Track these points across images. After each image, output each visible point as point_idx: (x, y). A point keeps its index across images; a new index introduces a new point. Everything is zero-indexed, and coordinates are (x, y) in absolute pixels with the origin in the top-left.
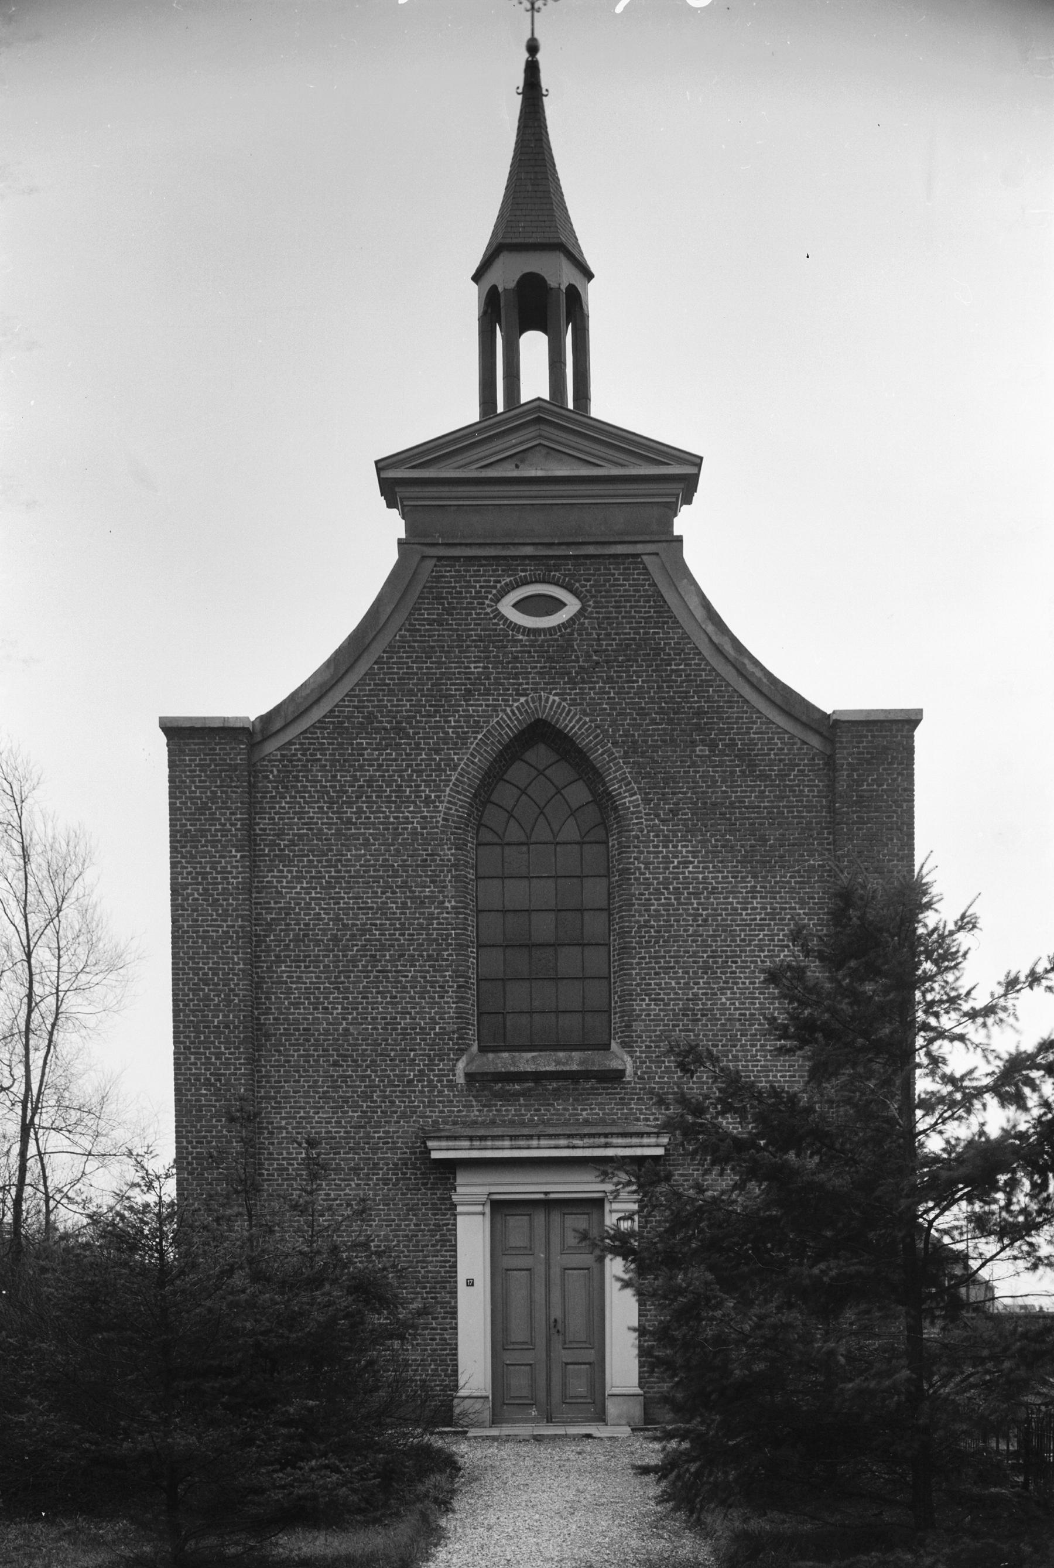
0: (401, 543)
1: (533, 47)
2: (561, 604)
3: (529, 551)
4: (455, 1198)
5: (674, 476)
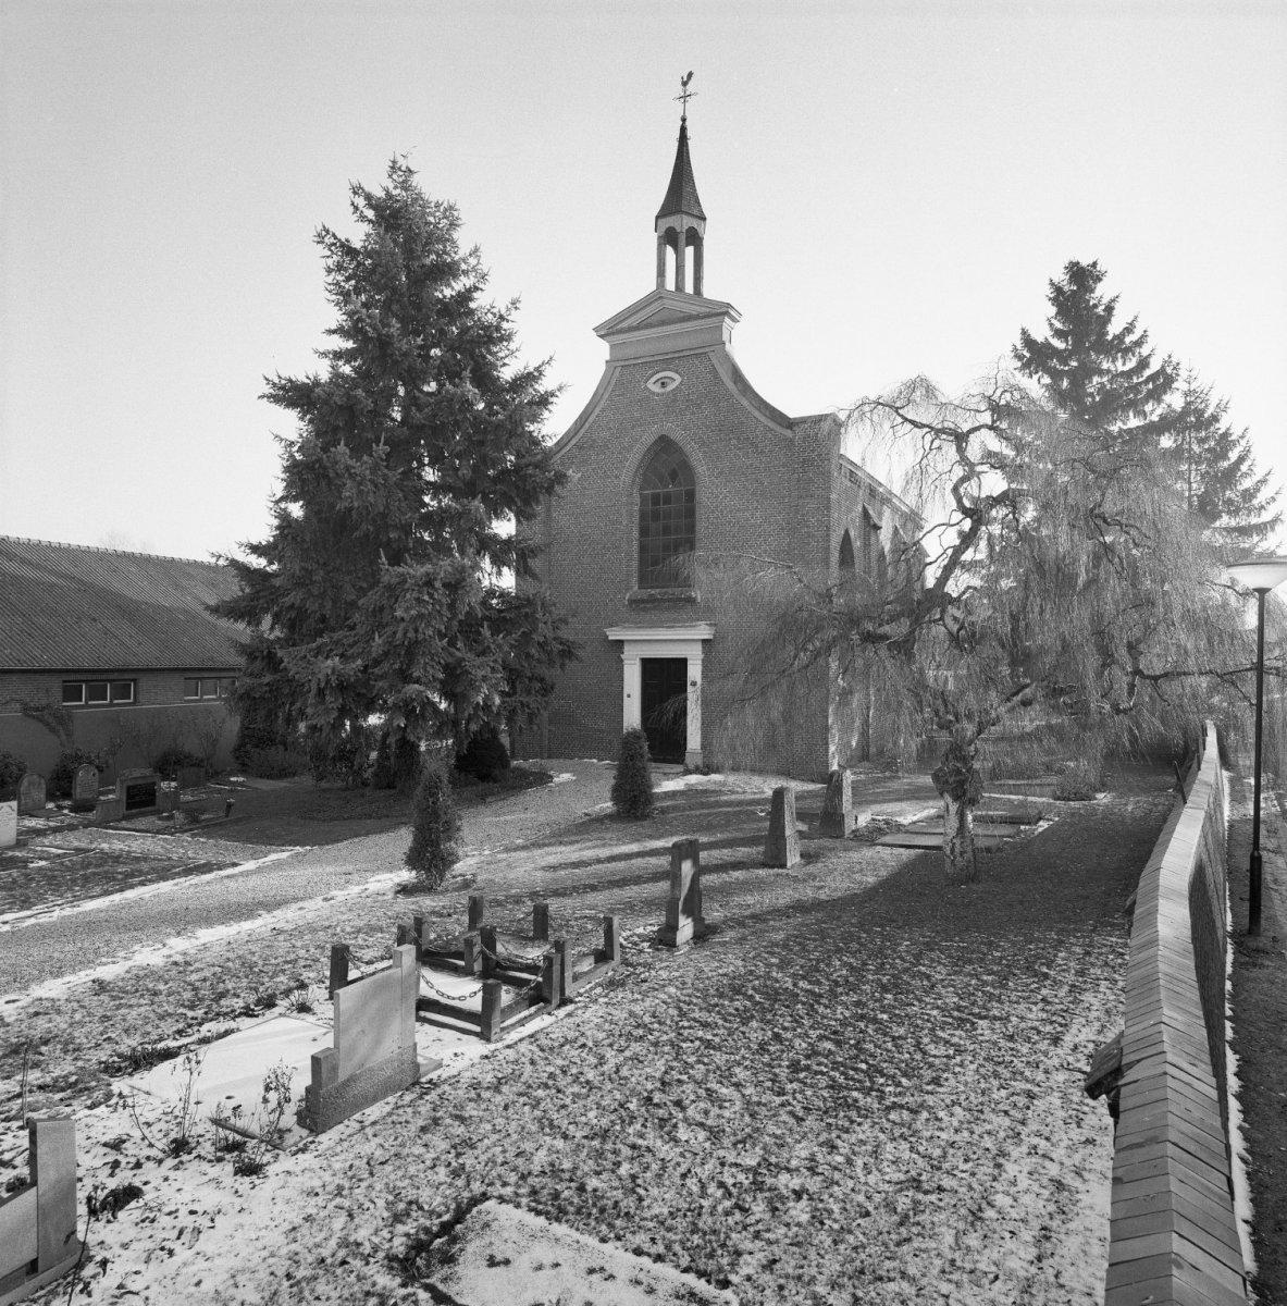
1: (684, 120)
5: (723, 311)
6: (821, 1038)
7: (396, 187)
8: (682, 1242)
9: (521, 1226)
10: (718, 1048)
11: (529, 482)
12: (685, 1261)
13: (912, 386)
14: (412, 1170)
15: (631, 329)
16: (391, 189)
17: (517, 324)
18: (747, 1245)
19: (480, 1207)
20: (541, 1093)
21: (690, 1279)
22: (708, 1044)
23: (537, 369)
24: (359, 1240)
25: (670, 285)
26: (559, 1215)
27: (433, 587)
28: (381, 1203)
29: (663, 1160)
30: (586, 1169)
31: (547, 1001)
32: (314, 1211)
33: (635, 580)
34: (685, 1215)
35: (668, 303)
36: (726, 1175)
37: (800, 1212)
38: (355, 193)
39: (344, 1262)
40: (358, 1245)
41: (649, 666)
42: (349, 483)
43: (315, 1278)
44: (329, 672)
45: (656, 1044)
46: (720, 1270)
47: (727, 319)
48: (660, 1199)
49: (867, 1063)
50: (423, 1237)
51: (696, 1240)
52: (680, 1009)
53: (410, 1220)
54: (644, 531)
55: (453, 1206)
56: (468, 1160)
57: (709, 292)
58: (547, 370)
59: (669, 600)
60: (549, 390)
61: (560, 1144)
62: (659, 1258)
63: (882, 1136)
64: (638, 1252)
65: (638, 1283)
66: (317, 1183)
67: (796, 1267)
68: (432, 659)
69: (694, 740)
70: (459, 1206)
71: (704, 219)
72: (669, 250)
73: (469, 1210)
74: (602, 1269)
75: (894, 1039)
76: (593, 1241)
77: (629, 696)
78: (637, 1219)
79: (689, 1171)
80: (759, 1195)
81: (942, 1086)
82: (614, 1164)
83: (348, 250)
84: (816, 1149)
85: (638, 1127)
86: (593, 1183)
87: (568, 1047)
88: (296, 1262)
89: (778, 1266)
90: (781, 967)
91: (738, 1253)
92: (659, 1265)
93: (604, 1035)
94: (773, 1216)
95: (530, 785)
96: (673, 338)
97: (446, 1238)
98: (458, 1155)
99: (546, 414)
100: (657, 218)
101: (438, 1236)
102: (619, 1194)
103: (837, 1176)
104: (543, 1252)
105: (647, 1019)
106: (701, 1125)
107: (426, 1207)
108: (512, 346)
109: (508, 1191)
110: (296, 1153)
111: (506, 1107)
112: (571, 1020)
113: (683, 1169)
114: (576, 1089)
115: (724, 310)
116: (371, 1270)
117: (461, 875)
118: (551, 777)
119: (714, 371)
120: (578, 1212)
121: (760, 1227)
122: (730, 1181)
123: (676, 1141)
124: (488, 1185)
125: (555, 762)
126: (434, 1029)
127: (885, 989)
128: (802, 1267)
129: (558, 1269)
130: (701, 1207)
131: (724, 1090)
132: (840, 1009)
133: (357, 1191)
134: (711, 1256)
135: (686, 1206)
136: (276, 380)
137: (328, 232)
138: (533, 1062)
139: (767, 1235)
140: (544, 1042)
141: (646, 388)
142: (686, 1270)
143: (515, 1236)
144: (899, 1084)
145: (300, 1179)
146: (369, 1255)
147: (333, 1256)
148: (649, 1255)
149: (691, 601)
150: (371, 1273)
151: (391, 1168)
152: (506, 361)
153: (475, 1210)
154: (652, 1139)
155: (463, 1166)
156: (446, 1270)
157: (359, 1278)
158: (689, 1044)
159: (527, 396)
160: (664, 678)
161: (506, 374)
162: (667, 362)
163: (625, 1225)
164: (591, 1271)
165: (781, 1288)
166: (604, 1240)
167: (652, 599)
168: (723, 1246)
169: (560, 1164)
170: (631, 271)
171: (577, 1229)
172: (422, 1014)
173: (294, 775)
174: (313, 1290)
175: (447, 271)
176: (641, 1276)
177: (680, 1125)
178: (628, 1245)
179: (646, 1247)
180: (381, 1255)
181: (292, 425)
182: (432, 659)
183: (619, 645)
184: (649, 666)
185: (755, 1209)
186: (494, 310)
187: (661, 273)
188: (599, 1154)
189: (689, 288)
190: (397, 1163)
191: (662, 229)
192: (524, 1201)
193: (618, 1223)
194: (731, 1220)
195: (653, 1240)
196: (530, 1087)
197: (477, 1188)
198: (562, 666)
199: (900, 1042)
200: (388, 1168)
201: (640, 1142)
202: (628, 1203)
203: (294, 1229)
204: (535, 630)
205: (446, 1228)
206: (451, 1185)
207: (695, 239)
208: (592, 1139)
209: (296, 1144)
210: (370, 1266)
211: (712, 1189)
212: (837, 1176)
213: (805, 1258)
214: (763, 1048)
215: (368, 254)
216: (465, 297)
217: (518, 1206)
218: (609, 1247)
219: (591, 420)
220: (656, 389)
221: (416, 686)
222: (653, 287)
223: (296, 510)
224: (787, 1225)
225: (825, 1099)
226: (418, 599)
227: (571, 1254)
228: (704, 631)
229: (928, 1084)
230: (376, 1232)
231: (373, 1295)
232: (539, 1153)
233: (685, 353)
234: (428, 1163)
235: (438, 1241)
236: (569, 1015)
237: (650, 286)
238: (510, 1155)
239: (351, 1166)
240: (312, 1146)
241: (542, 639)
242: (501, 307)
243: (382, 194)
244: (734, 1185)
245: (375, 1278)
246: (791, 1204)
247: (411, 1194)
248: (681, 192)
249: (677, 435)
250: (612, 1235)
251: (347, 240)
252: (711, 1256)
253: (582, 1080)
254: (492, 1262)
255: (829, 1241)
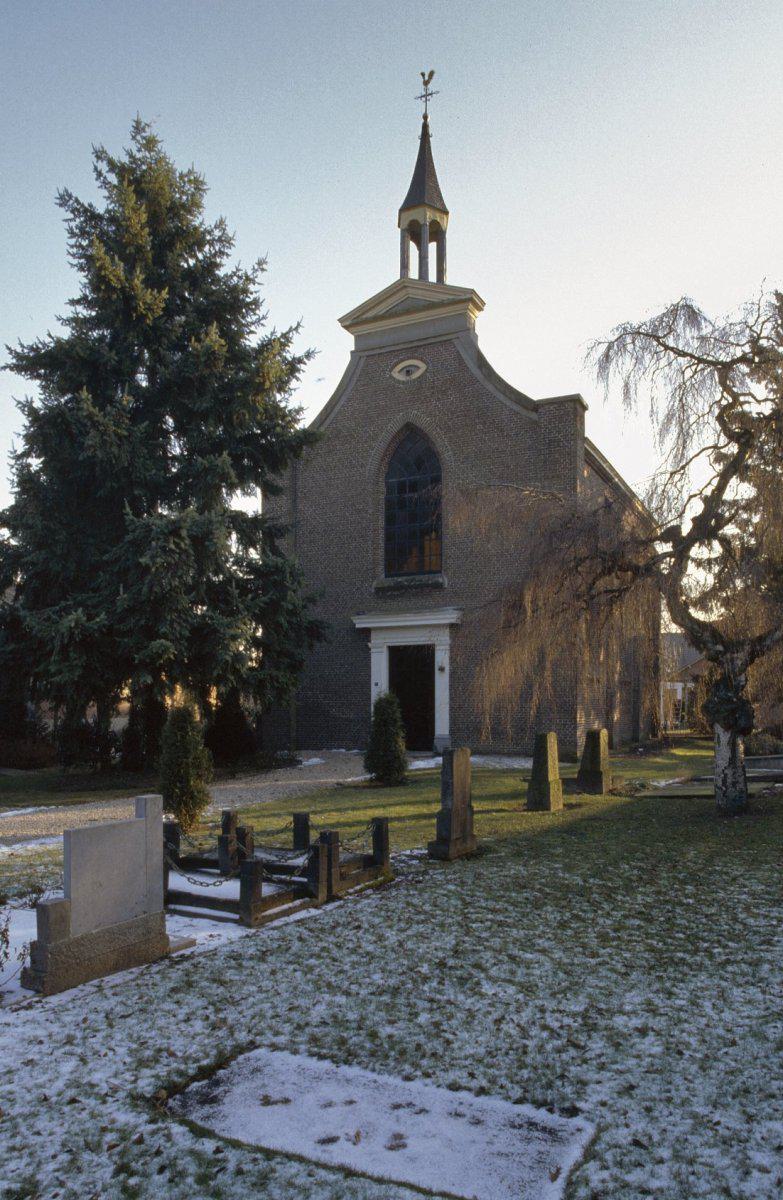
0: (352, 352)
1: (425, 117)
2: (418, 368)
3: (402, 346)
4: (370, 645)
5: (468, 300)
6: (626, 917)
7: (139, 151)
8: (507, 1076)
9: (301, 1071)
10: (515, 926)
11: (271, 451)
12: (517, 1092)
13: (674, 311)
14: (161, 1022)
15: (376, 319)
16: (135, 152)
17: (263, 290)
18: (593, 1076)
19: (247, 1055)
20: (312, 961)
21: (527, 1110)
22: (501, 924)
23: (284, 336)
24: (93, 1082)
25: (414, 274)
26: (350, 1058)
27: (179, 536)
28: (121, 1051)
29: (469, 1010)
30: (376, 1018)
31: (313, 895)
32: (36, 1057)
33: (381, 568)
34: (507, 1054)
35: (412, 293)
36: (549, 1020)
37: (651, 1046)
38: (98, 157)
39: (73, 1101)
40: (92, 1086)
41: (397, 655)
42: (93, 432)
43: (34, 1115)
44: (73, 625)
45: (442, 925)
46: (564, 1098)
47: (471, 306)
48: (470, 1043)
49: (684, 933)
50: (176, 1079)
51: (525, 1073)
52: (463, 900)
53: (158, 1066)
54: (390, 520)
55: (214, 1052)
56: (231, 1015)
57: (451, 280)
58: (295, 337)
59: (416, 587)
60: (297, 356)
61: (341, 999)
62: (482, 1091)
63: (724, 984)
64: (454, 1087)
65: (458, 1115)
66: (41, 1033)
67: (660, 1092)
68: (179, 617)
69: (442, 726)
70: (220, 1053)
71: (447, 213)
72: (413, 247)
73: (233, 1057)
74: (410, 1105)
75: (706, 916)
76: (395, 1081)
77: (377, 684)
78: (447, 1059)
79: (503, 1018)
80: (594, 1034)
81: (775, 946)
82: (411, 1014)
83: (90, 215)
84: (651, 995)
85: (434, 984)
86: (385, 1031)
87: (339, 929)
88: (9, 1100)
89: (637, 1091)
90: (568, 868)
91: (584, 1083)
92: (482, 1099)
93: (381, 919)
94: (617, 1050)
95: (280, 767)
96: (419, 333)
97: (204, 1082)
98: (218, 1011)
99: (293, 384)
100: (401, 211)
101: (194, 1079)
102: (422, 1039)
103: (683, 1015)
104: (329, 1091)
105: (427, 907)
106: (510, 981)
107: (179, 1054)
108: (261, 312)
109: (282, 1039)
110: (16, 1010)
111: (273, 973)
112: (343, 910)
113: (496, 1015)
114: (354, 958)
115: (468, 296)
116: (110, 1107)
117: (212, 822)
118: (301, 761)
119: (461, 361)
120: (372, 1054)
121: (603, 1059)
122: (556, 1025)
123: (482, 996)
124: (257, 1035)
125: (303, 752)
126: (187, 920)
127: (684, 882)
128: (669, 1091)
129: (353, 1106)
130: (525, 1046)
131: (529, 956)
132: (639, 897)
133: (91, 1040)
134: (549, 1085)
135: (508, 1046)
136: (19, 350)
137: (70, 196)
138: (300, 939)
139: (615, 1067)
140: (312, 925)
141: (391, 377)
142: (519, 1101)
143: (294, 1078)
144: (726, 947)
145: (20, 1030)
146: (106, 1095)
147: (59, 1095)
148: (470, 1090)
149: (439, 586)
150: (109, 1110)
151: (135, 1021)
152: (253, 328)
153: (241, 1058)
154: (450, 992)
155: (224, 1020)
156: (207, 1109)
157: (93, 1116)
158: (480, 924)
159: (276, 365)
160: (412, 666)
161: (252, 341)
162: (413, 350)
163: (432, 1064)
164: (397, 1107)
165: (648, 1110)
166: (408, 1078)
167: (399, 587)
168: (562, 1077)
169: (344, 1016)
170: (375, 264)
171: (373, 1070)
172: (172, 907)
173: (43, 766)
174: (32, 1126)
175: (196, 239)
176: (461, 1109)
177: (484, 982)
178: (441, 1081)
179: (464, 1081)
180: (121, 1094)
181: (32, 390)
182: (179, 617)
183: (366, 633)
184: (397, 655)
185: (591, 1044)
186: (240, 273)
187: (405, 266)
188: (390, 1007)
189: (432, 277)
190: (143, 1017)
191: (405, 224)
192: (303, 1047)
193: (425, 1062)
194: (564, 1056)
195: (472, 1075)
196: (300, 957)
197: (242, 1037)
198: (311, 646)
199: (715, 918)
200: (131, 1021)
201: (438, 997)
202: (437, 1045)
203: (10, 1072)
204: (284, 598)
205: (205, 1073)
206: (209, 1036)
207: (438, 234)
208: (380, 994)
209: (17, 1003)
210: (108, 1105)
211: (534, 1031)
212: (683, 1015)
213: (670, 1083)
214: (563, 925)
215: (113, 220)
216: (210, 266)
217: (295, 1052)
218: (416, 1085)
219: (336, 410)
220: (401, 377)
221: (163, 641)
222: (397, 277)
223: (35, 463)
224: (638, 1056)
225: (647, 960)
226: (163, 549)
227: (368, 1092)
228: (450, 616)
229: (760, 945)
230: (116, 1075)
231: (111, 1131)
232: (317, 1007)
233: (430, 341)
234: (181, 1017)
235: (195, 1085)
236: (341, 907)
237: (394, 276)
238: (282, 1009)
239: (85, 1020)
240: (39, 1005)
241: (291, 607)
242: (247, 268)
243: (126, 160)
244: (561, 1027)
245: (114, 1115)
246: (637, 1040)
247: (161, 1042)
248: (424, 190)
249: (423, 422)
250: (419, 1073)
251: (91, 205)
252: (549, 1085)
253: (361, 951)
254: (267, 1101)
255: (694, 1068)
